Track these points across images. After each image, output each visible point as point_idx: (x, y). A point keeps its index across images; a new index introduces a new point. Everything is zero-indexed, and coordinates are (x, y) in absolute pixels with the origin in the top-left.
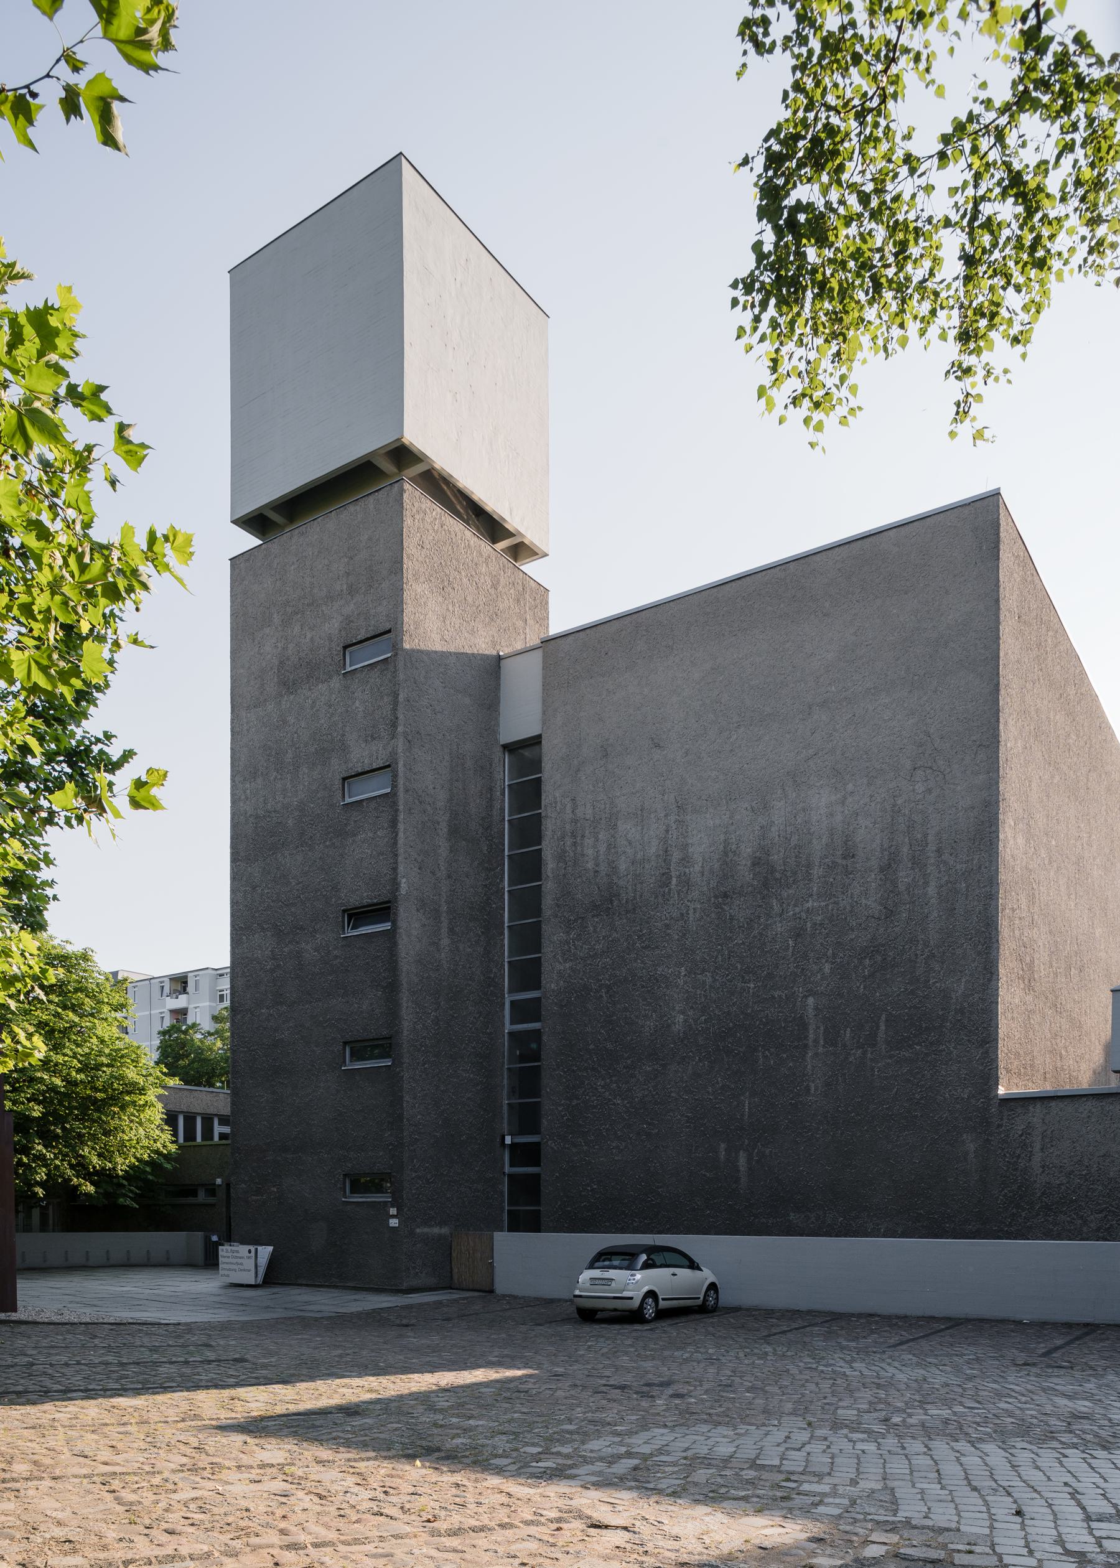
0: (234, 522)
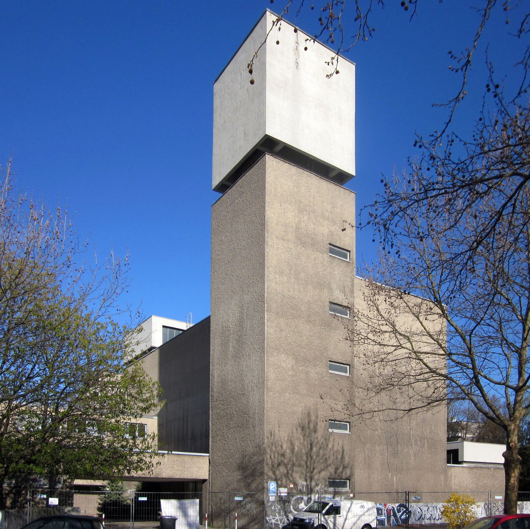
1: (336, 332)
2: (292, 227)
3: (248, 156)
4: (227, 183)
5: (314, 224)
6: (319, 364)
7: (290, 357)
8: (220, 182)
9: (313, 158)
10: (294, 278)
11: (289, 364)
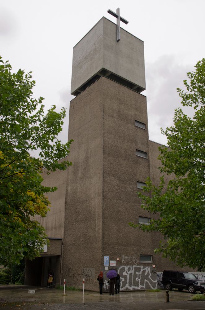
1: (140, 165)
2: (116, 111)
3: (95, 76)
4: (79, 91)
5: (127, 110)
6: (132, 183)
7: (116, 179)
8: (76, 90)
9: (125, 80)
10: (118, 136)
11: (116, 182)
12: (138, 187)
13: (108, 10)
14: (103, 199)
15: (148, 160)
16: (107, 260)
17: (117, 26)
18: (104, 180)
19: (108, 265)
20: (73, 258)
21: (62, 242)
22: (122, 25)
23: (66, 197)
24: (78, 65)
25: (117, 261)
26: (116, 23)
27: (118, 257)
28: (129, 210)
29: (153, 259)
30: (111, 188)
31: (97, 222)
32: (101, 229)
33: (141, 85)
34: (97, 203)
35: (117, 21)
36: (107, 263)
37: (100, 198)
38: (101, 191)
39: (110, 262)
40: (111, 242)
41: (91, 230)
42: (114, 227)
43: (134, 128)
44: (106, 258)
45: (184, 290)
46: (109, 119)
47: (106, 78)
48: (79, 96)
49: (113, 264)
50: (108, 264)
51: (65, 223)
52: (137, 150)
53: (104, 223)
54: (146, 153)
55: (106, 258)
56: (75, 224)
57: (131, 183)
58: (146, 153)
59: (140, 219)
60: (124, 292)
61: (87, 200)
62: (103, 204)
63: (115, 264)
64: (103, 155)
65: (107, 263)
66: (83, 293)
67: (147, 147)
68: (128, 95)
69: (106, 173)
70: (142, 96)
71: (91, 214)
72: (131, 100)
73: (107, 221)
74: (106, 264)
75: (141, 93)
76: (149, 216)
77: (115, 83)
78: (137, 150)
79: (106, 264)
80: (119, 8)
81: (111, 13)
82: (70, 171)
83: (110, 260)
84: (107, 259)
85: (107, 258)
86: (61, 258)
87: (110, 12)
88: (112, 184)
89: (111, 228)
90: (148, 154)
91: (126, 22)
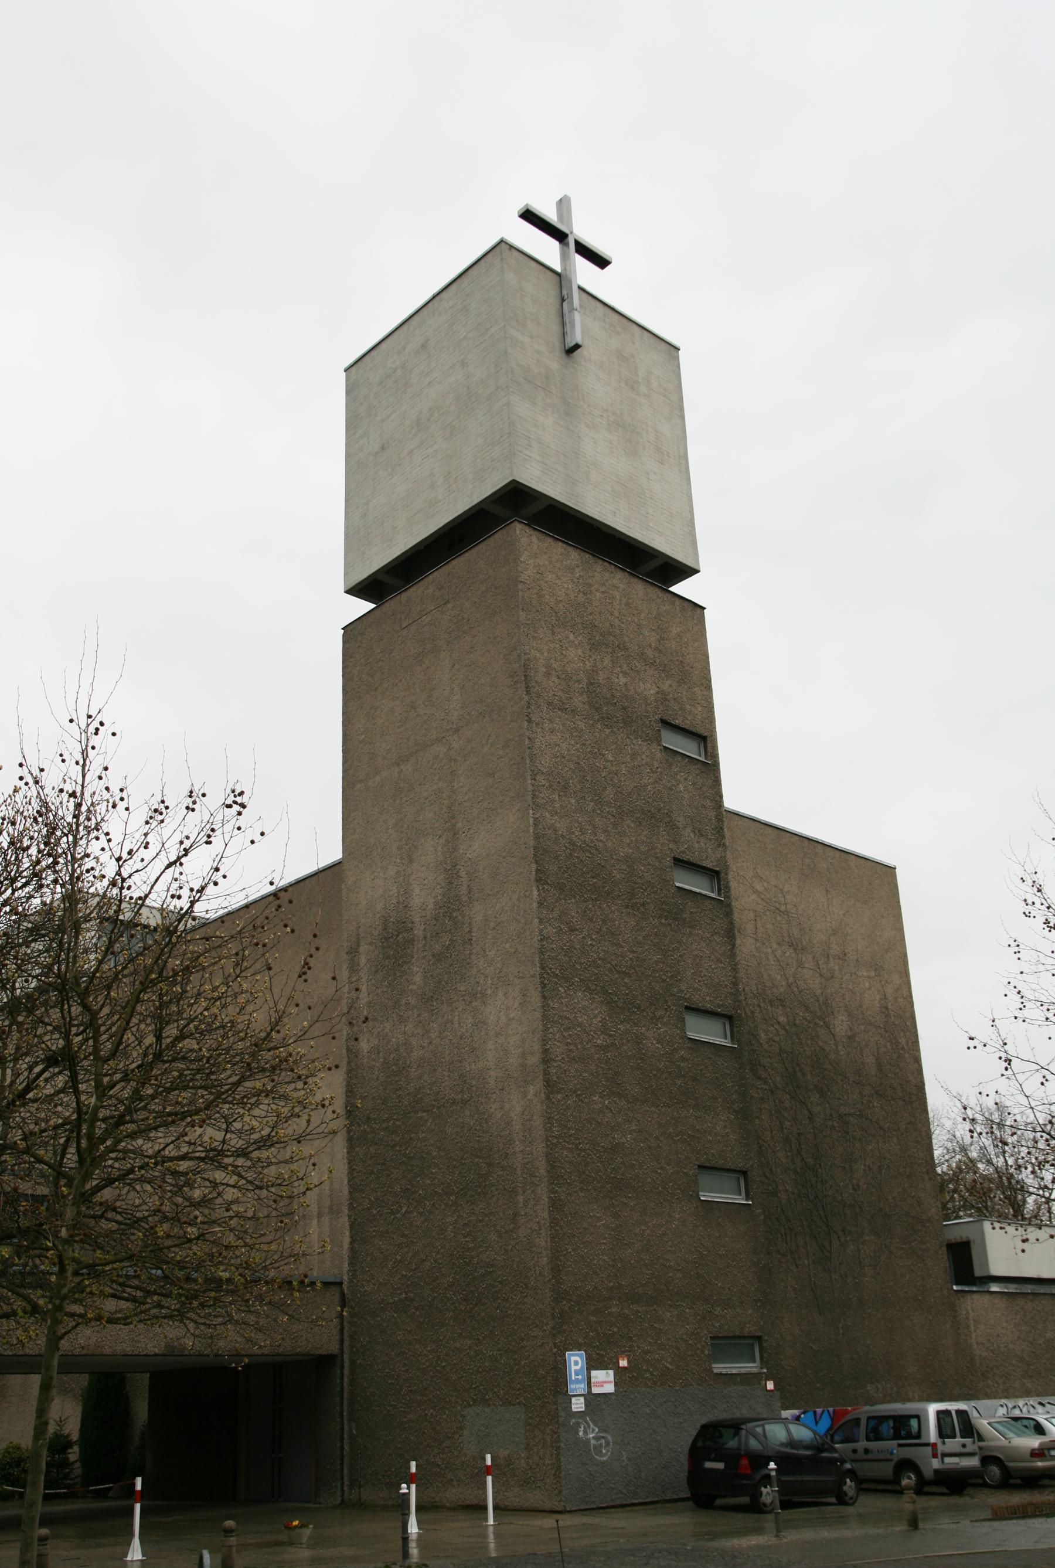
0: (348, 592)
2: (579, 682)
5: (625, 674)
10: (592, 800)
11: (596, 1016)
12: (691, 1035)
13: (520, 207)
14: (548, 1098)
15: (725, 906)
16: (578, 1367)
17: (561, 279)
18: (545, 1006)
19: (581, 1388)
20: (405, 1365)
21: (343, 1294)
22: (584, 272)
23: (348, 1085)
24: (376, 454)
25: (619, 1372)
26: (559, 270)
27: (623, 1352)
28: (657, 1138)
29: (765, 1355)
30: (576, 1045)
31: (521, 1198)
32: (543, 1232)
33: (680, 555)
34: (517, 1110)
35: (565, 257)
36: (577, 1381)
37: (532, 1090)
38: (534, 1060)
39: (589, 1378)
40: (589, 1288)
41: (493, 1237)
42: (599, 1219)
43: (659, 756)
44: (573, 1359)
45: (973, 1481)
46: (551, 721)
47: (527, 529)
48: (392, 605)
49: (601, 1384)
50: (582, 1386)
51: (351, 1204)
52: (679, 862)
53: (556, 1205)
54: (715, 875)
55: (573, 1359)
56: (404, 1210)
57: (658, 1013)
58: (717, 873)
59: (705, 1179)
60: (635, 1508)
61: (465, 1102)
62: (549, 1120)
63: (609, 1382)
64: (535, 893)
65: (577, 1381)
66: (486, 1519)
67: (719, 846)
68: (627, 604)
69: (554, 976)
70: (686, 604)
71: (489, 1165)
72: (639, 626)
73: (571, 1195)
74: (576, 1387)
75: (673, 589)
76: (741, 1165)
77: (570, 549)
78: (679, 862)
79: (573, 1386)
80: (569, 194)
81: (535, 220)
82: (363, 961)
83: (589, 1370)
84: (576, 1363)
85: (577, 1358)
86: (342, 1367)
87: (529, 216)
88: (580, 1025)
89: (585, 1225)
90: (722, 875)
91: (602, 262)
